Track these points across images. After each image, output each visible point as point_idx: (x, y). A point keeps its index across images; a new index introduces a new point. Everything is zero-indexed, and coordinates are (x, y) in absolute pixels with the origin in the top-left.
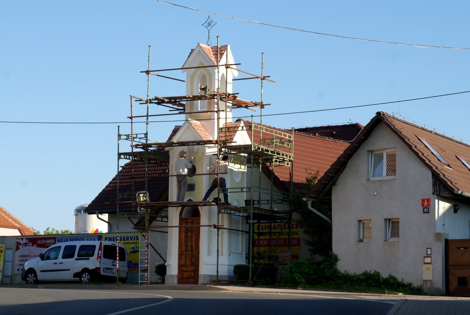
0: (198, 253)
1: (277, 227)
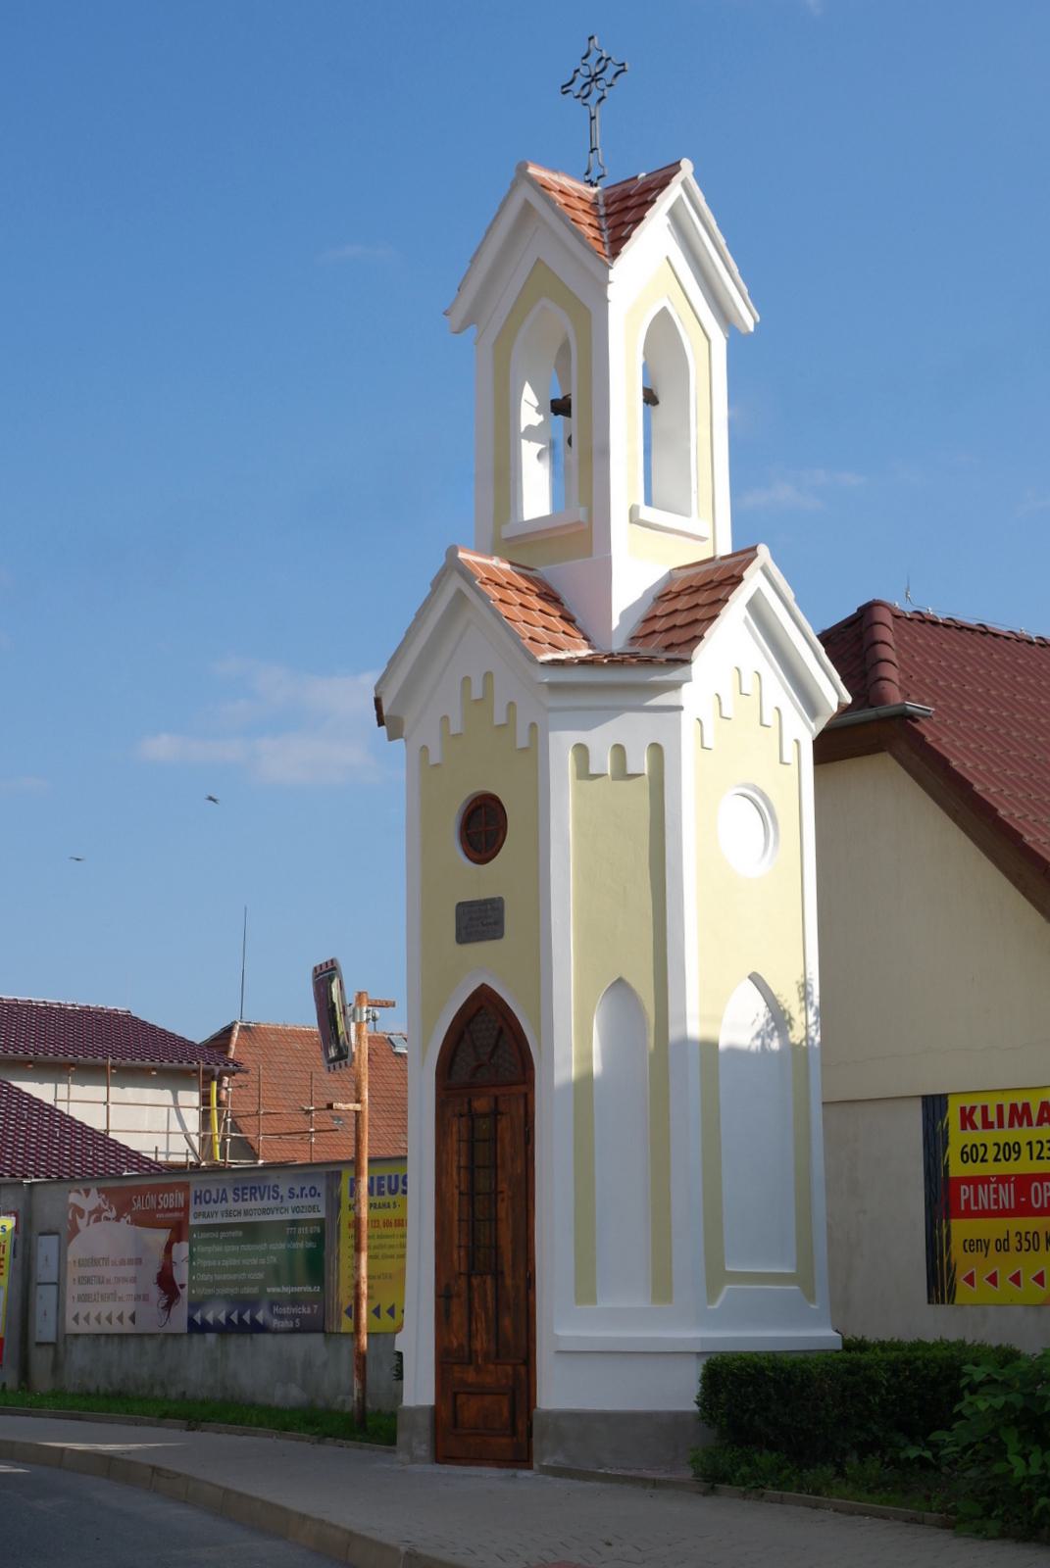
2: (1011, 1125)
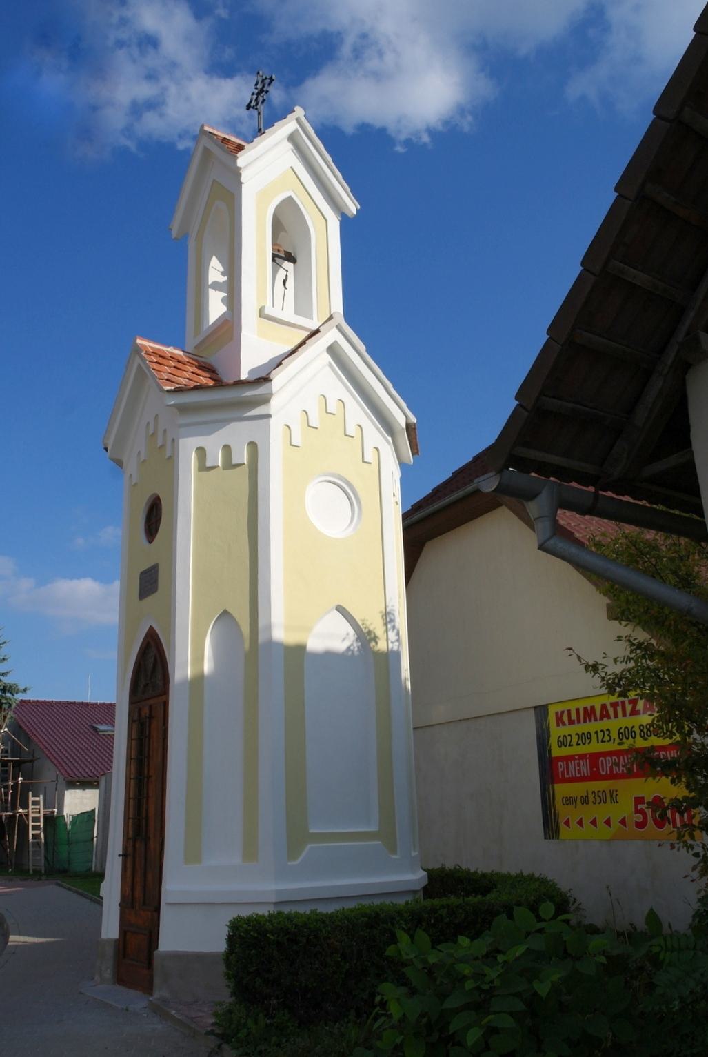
1: (611, 711)
2: (585, 721)
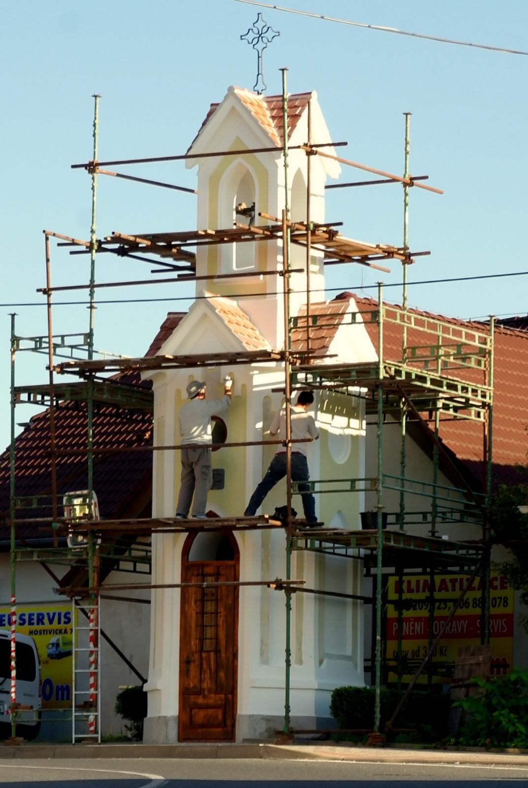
0: (235, 656)
1: (450, 585)
